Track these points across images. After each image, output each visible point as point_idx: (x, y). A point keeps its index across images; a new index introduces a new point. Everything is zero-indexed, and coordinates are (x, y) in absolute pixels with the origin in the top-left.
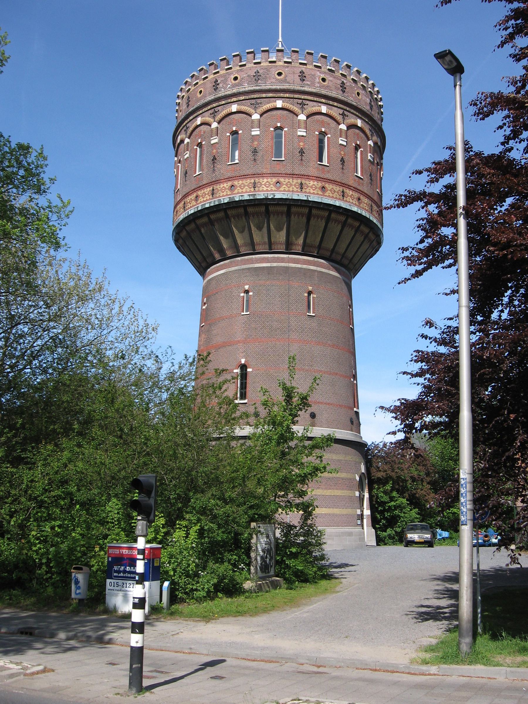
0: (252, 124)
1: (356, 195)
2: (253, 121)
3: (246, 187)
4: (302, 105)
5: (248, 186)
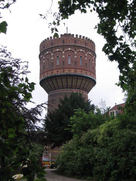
0: (75, 55)
1: (90, 73)
2: (75, 54)
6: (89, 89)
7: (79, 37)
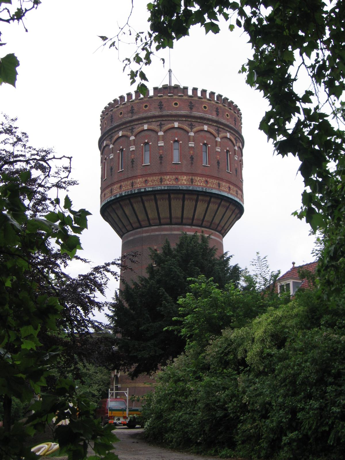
3: (156, 182)
4: (192, 126)
5: (196, 181)
6: (226, 227)
7: (199, 94)
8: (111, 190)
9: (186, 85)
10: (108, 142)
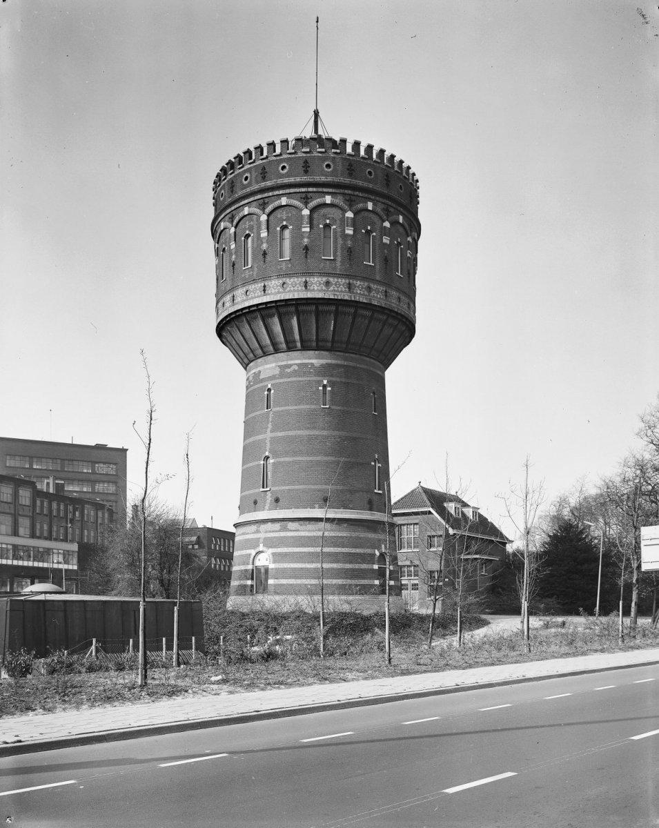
5: (343, 285)
8: (234, 296)
9: (344, 136)
10: (228, 224)
